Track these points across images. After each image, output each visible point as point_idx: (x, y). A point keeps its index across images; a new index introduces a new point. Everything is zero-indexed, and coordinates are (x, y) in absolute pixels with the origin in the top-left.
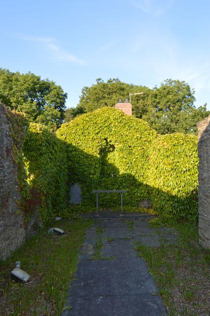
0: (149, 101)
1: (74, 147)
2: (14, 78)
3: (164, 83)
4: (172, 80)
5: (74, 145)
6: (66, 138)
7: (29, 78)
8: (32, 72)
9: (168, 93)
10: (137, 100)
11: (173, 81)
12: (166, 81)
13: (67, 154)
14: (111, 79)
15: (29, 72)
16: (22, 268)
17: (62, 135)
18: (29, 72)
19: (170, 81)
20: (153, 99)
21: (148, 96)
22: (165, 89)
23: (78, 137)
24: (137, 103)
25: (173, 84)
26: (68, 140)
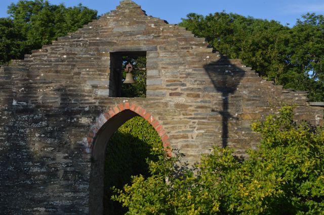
0: (273, 53)
1: (140, 141)
2: (57, 17)
3: (303, 20)
4: (316, 15)
5: (141, 138)
6: (131, 130)
7: (80, 15)
8: (83, 5)
9: (307, 38)
10: (254, 50)
11: (318, 17)
12: (304, 17)
13: (132, 150)
14: (211, 15)
15: (80, 5)
16: (238, 157)
17: (127, 127)
18: (80, 5)
19: (313, 17)
20: (283, 47)
21: (273, 43)
22: (302, 30)
23: (145, 129)
24: (254, 55)
25: (318, 21)
26: (133, 133)
